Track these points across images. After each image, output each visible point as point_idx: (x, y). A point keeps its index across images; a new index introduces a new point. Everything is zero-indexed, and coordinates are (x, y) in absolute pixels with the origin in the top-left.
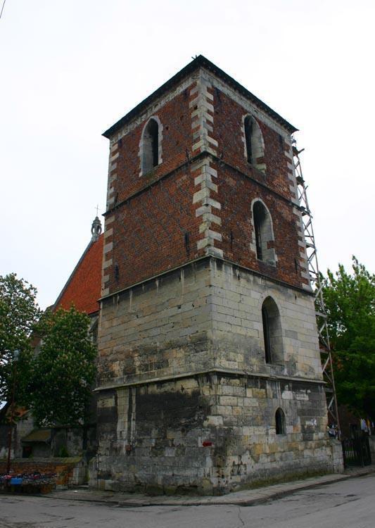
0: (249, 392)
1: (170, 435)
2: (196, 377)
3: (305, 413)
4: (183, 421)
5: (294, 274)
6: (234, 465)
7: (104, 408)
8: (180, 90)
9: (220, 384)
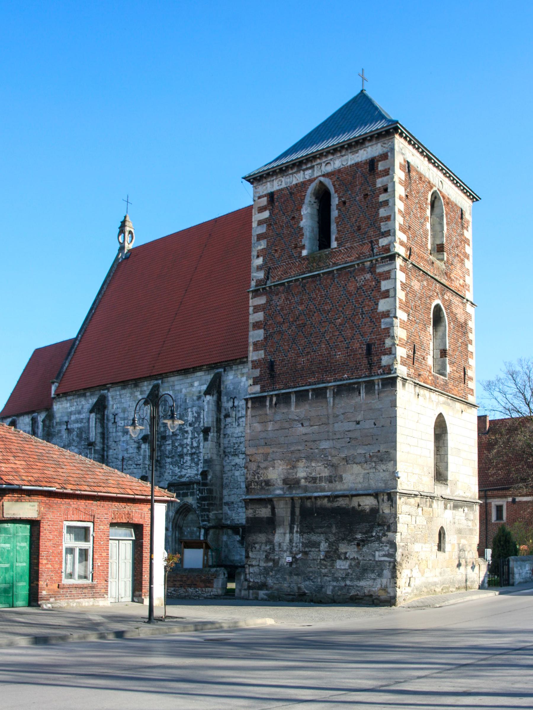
1: (343, 548)
4: (359, 536)
5: (462, 385)
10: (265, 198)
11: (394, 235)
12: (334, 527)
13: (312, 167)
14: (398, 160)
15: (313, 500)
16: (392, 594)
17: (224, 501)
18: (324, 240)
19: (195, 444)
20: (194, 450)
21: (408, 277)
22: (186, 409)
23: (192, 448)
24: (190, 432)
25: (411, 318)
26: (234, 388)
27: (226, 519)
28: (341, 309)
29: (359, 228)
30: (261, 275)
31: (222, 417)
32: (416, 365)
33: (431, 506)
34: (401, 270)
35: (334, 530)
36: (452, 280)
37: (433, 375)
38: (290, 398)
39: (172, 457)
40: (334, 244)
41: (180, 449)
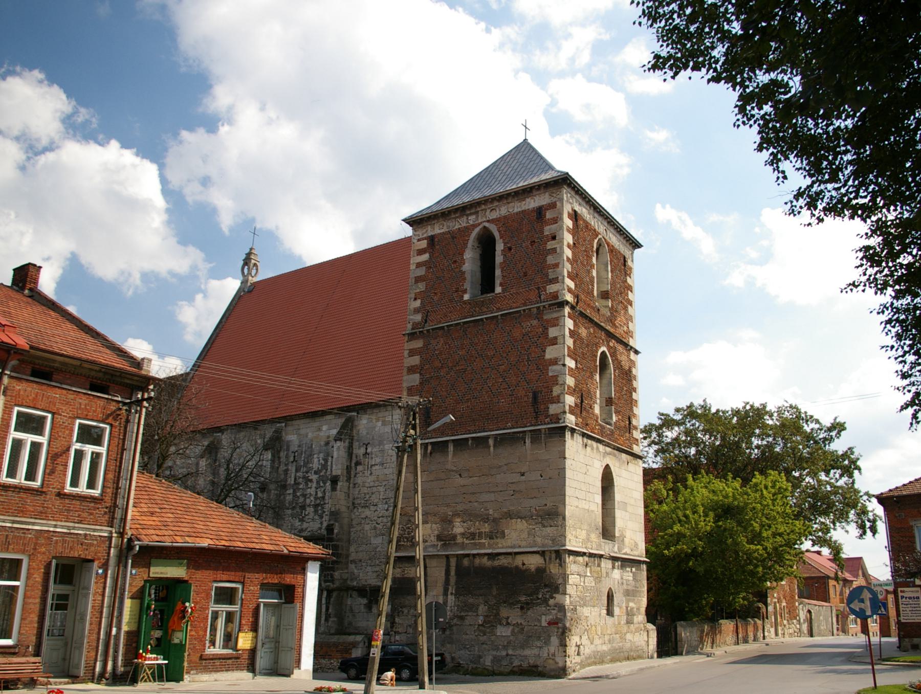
1: (504, 612)
2: (542, 554)
3: (629, 594)
4: (523, 598)
5: (627, 435)
7: (404, 578)
8: (532, 203)
10: (425, 241)
11: (563, 283)
12: (495, 589)
13: (477, 213)
14: (567, 209)
15: (471, 558)
16: (561, 664)
17: (351, 559)
18: (487, 284)
19: (320, 495)
20: (318, 502)
21: (575, 325)
22: (311, 455)
23: (316, 498)
24: (315, 481)
25: (579, 365)
26: (368, 433)
27: (352, 580)
28: (505, 355)
29: (525, 274)
30: (418, 318)
31: (353, 465)
32: (584, 413)
33: (599, 565)
34: (569, 317)
35: (495, 592)
36: (616, 327)
37: (600, 425)
38: (447, 447)
39: (293, 508)
40: (498, 289)
41: (301, 500)
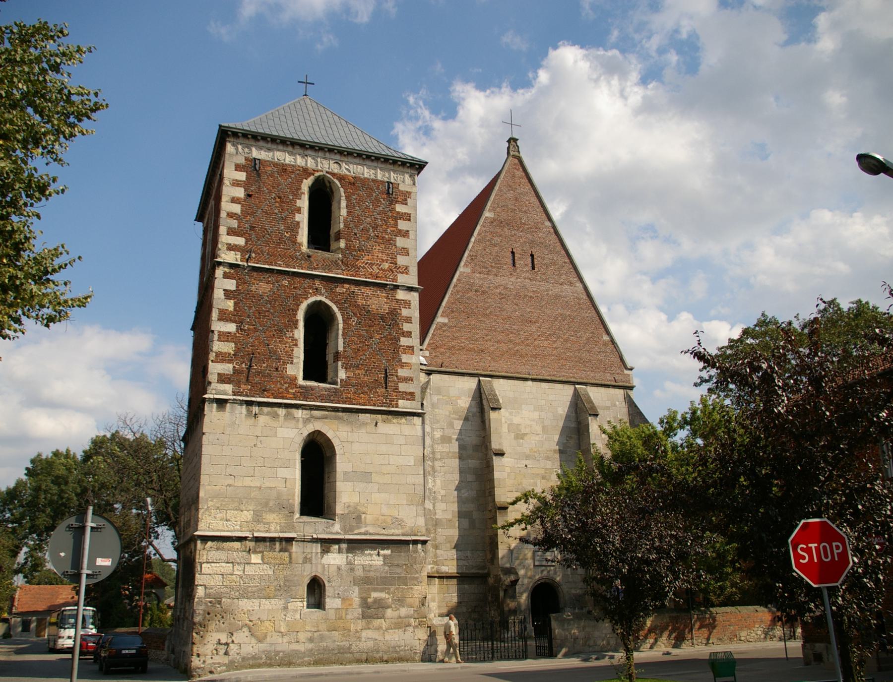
0: (255, 558)
6: (219, 643)
9: (204, 549)
